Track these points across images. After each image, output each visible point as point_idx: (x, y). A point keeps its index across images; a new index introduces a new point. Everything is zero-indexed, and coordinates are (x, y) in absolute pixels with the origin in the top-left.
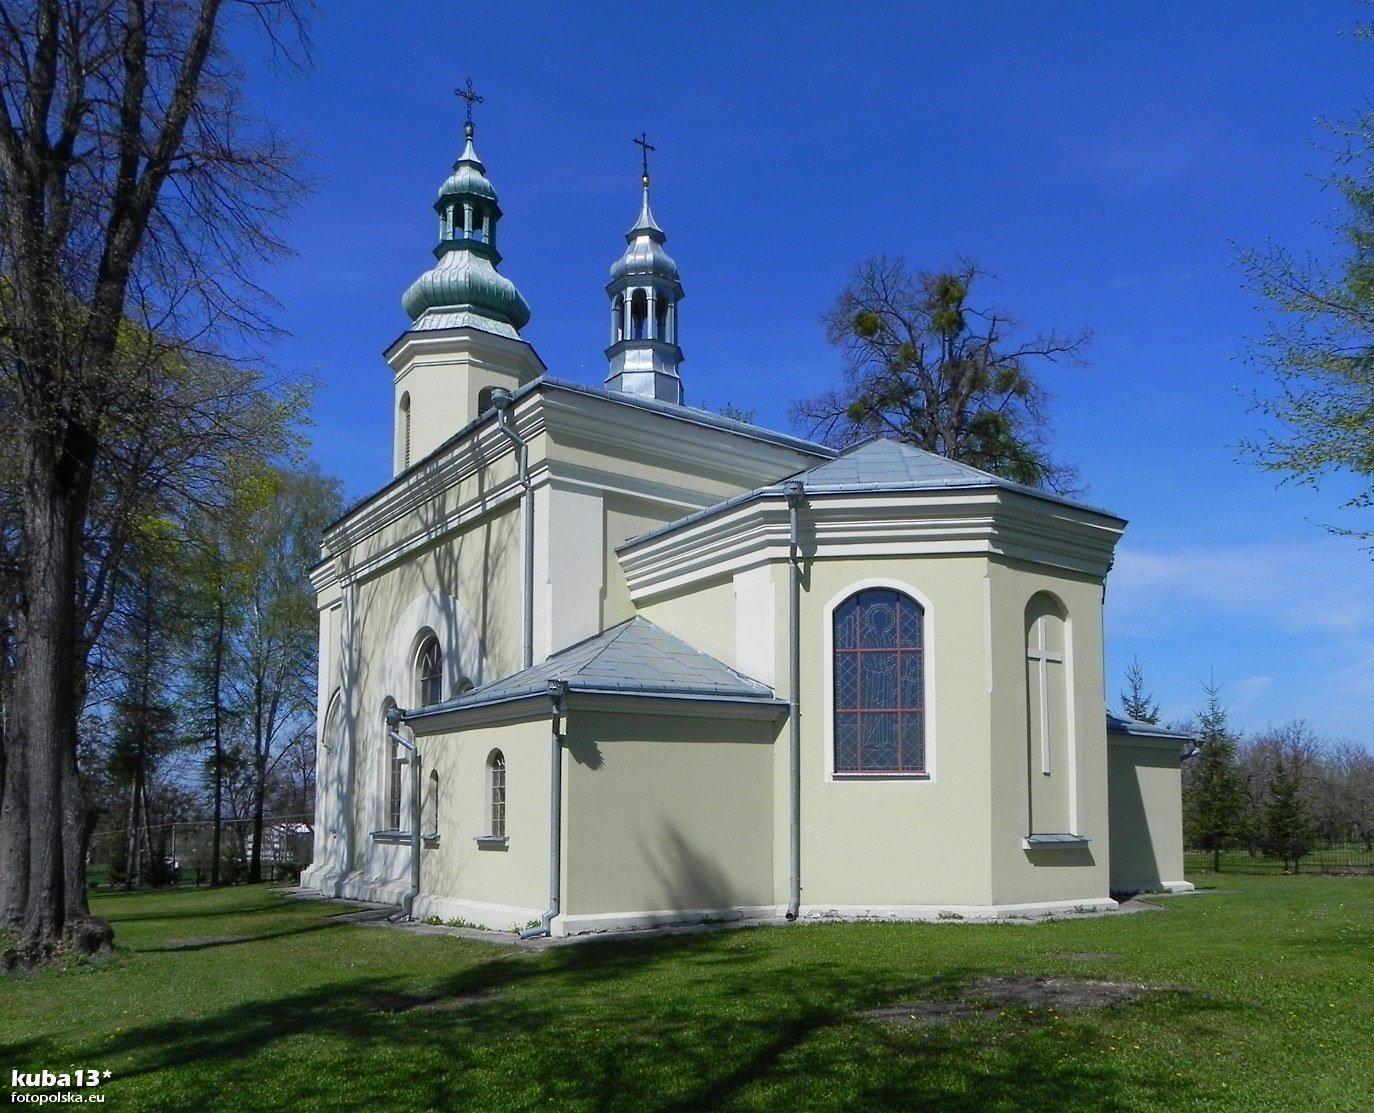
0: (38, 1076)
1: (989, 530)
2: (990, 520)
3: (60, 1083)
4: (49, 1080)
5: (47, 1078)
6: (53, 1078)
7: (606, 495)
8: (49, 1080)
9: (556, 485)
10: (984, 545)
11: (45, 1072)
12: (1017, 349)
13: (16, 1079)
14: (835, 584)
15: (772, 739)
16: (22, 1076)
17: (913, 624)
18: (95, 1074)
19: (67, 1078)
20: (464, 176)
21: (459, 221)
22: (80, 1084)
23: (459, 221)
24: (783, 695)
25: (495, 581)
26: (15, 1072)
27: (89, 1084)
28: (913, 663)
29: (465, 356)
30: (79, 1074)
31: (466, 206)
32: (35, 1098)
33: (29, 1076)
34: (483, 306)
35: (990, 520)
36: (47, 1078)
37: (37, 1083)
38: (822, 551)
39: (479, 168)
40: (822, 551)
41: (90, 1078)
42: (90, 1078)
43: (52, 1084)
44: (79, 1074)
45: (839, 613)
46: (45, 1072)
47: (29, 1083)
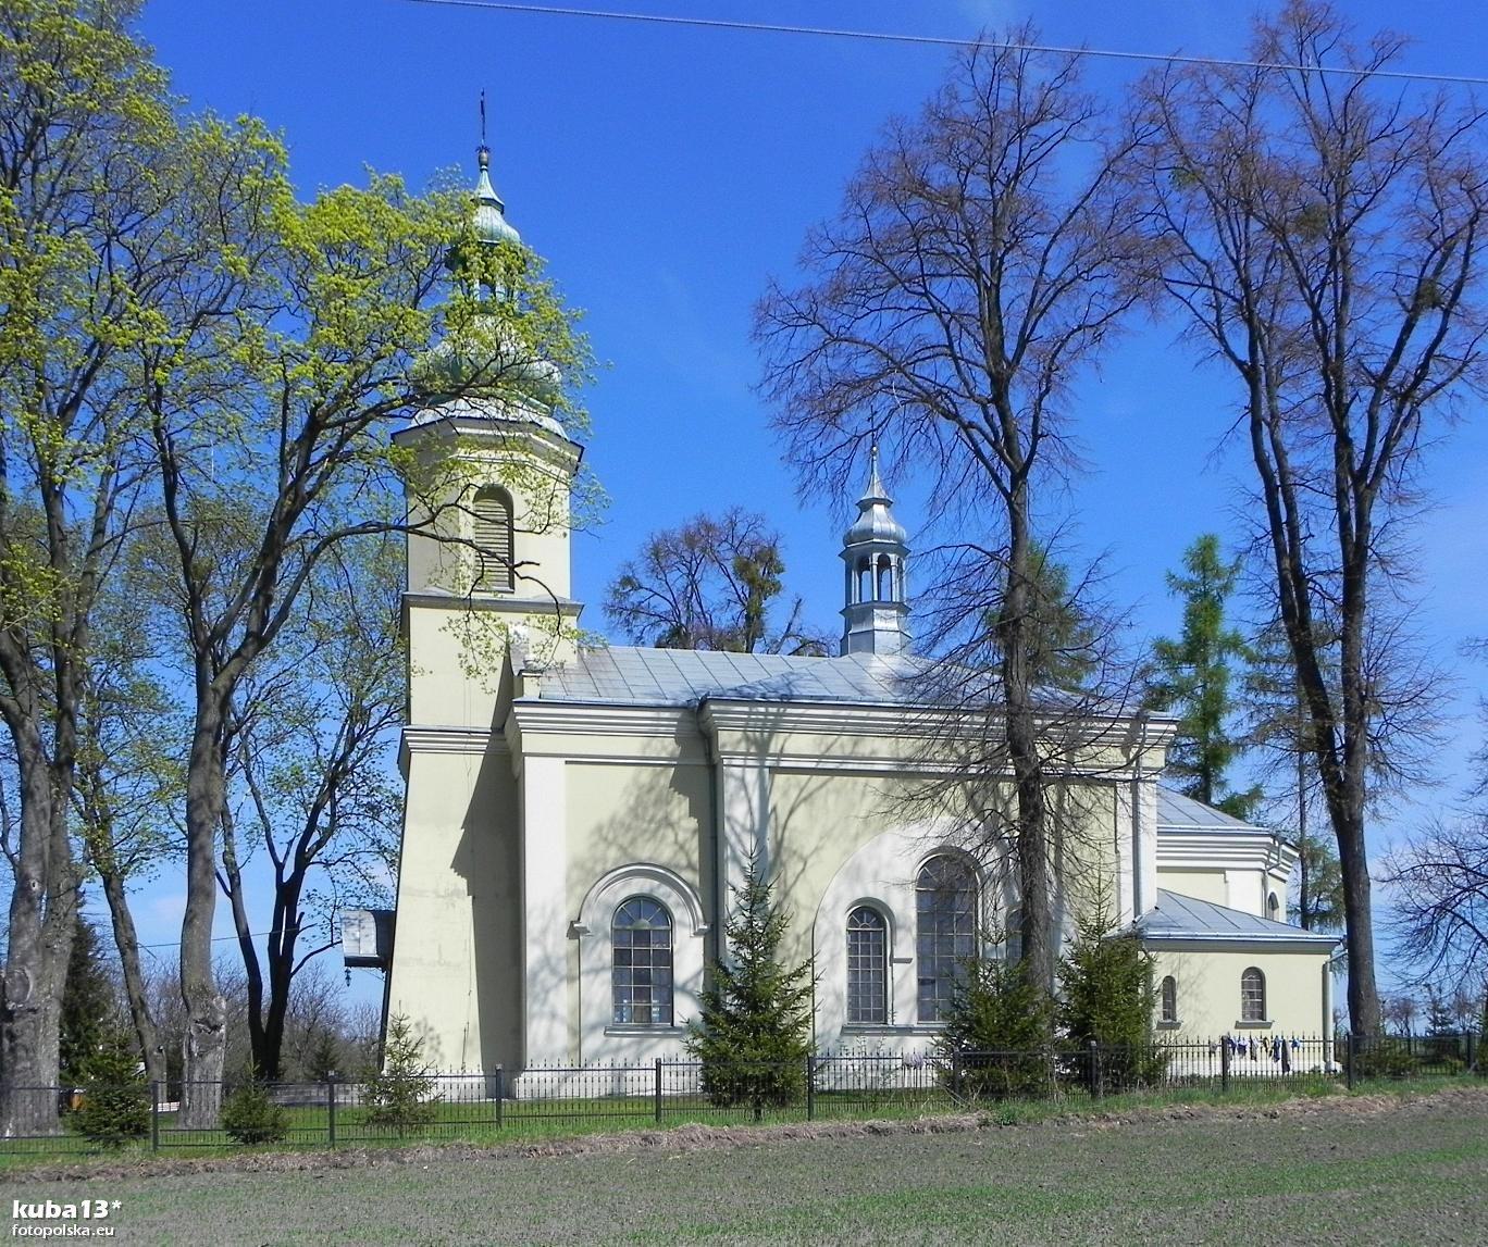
0: (41, 1207)
3: (65, 1215)
5: (50, 1209)
11: (49, 1202)
13: (17, 1209)
18: (104, 1204)
19: (73, 1209)
22: (87, 1215)
26: (16, 1203)
27: (96, 1215)
33: (32, 1207)
43: (57, 1215)
44: (86, 1204)
46: (49, 1202)
47: (32, 1214)
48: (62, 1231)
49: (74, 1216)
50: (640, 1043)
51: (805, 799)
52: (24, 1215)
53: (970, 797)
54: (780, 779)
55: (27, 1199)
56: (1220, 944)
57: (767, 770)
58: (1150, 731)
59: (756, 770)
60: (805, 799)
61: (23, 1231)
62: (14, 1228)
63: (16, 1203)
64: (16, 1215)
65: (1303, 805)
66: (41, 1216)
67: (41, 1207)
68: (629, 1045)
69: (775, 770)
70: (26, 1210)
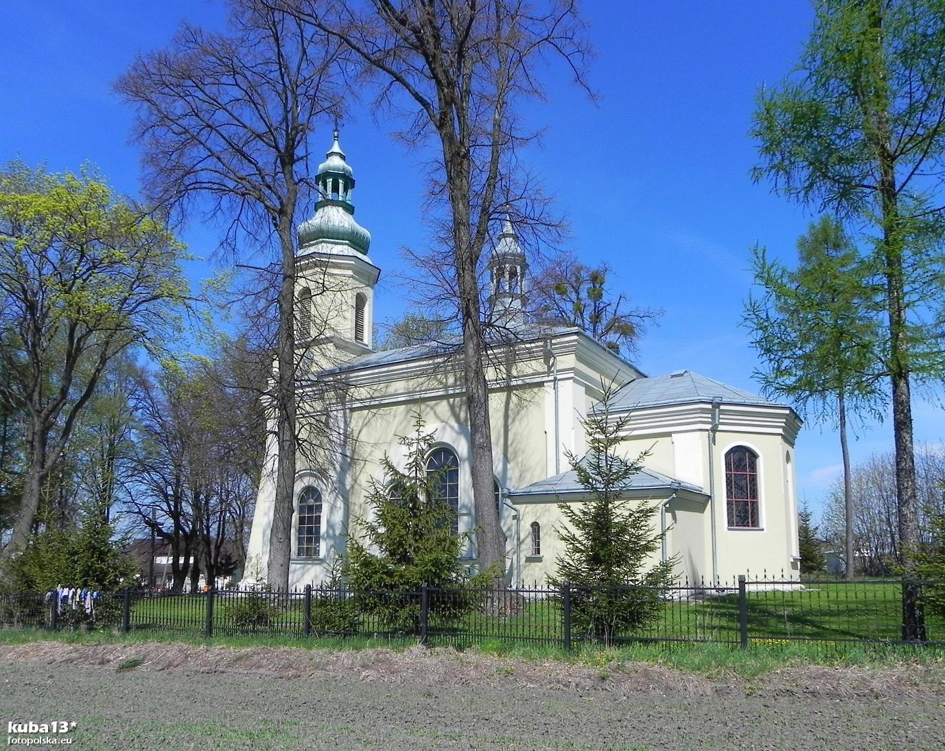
0: (26, 726)
1: (783, 425)
2: (784, 420)
3: (41, 731)
4: (33, 728)
5: (32, 727)
6: (36, 727)
7: (586, 386)
8: (33, 728)
9: (575, 381)
10: (780, 431)
11: (31, 723)
12: (628, 314)
13: (11, 727)
14: (726, 442)
15: (702, 511)
16: (15, 725)
17: (753, 463)
18: (66, 724)
19: (46, 727)
20: (335, 162)
21: (335, 189)
22: (55, 731)
23: (335, 189)
24: (707, 491)
25: (517, 423)
26: (10, 723)
27: (61, 731)
28: (753, 480)
29: (350, 272)
30: (54, 724)
31: (341, 181)
32: (24, 741)
33: (20, 726)
34: (357, 245)
35: (784, 420)
36: (32, 727)
37: (25, 730)
38: (721, 428)
39: (343, 158)
40: (721, 428)
41: (62, 727)
42: (62, 727)
43: (36, 731)
44: (54, 724)
45: (727, 455)
46: (31, 723)
47: (20, 730)
48: (39, 741)
49: (47, 731)
50: (303, 567)
51: (366, 424)
52: (15, 731)
53: (452, 407)
54: (355, 414)
55: (18, 721)
56: (573, 496)
57: (348, 411)
58: (555, 344)
59: (491, 148)
60: (366, 424)
61: (24, 741)
62: (9, 739)
63: (10, 723)
64: (10, 731)
65: (912, 173)
66: (26, 731)
67: (26, 726)
68: (299, 569)
69: (352, 410)
70: (17, 727)
